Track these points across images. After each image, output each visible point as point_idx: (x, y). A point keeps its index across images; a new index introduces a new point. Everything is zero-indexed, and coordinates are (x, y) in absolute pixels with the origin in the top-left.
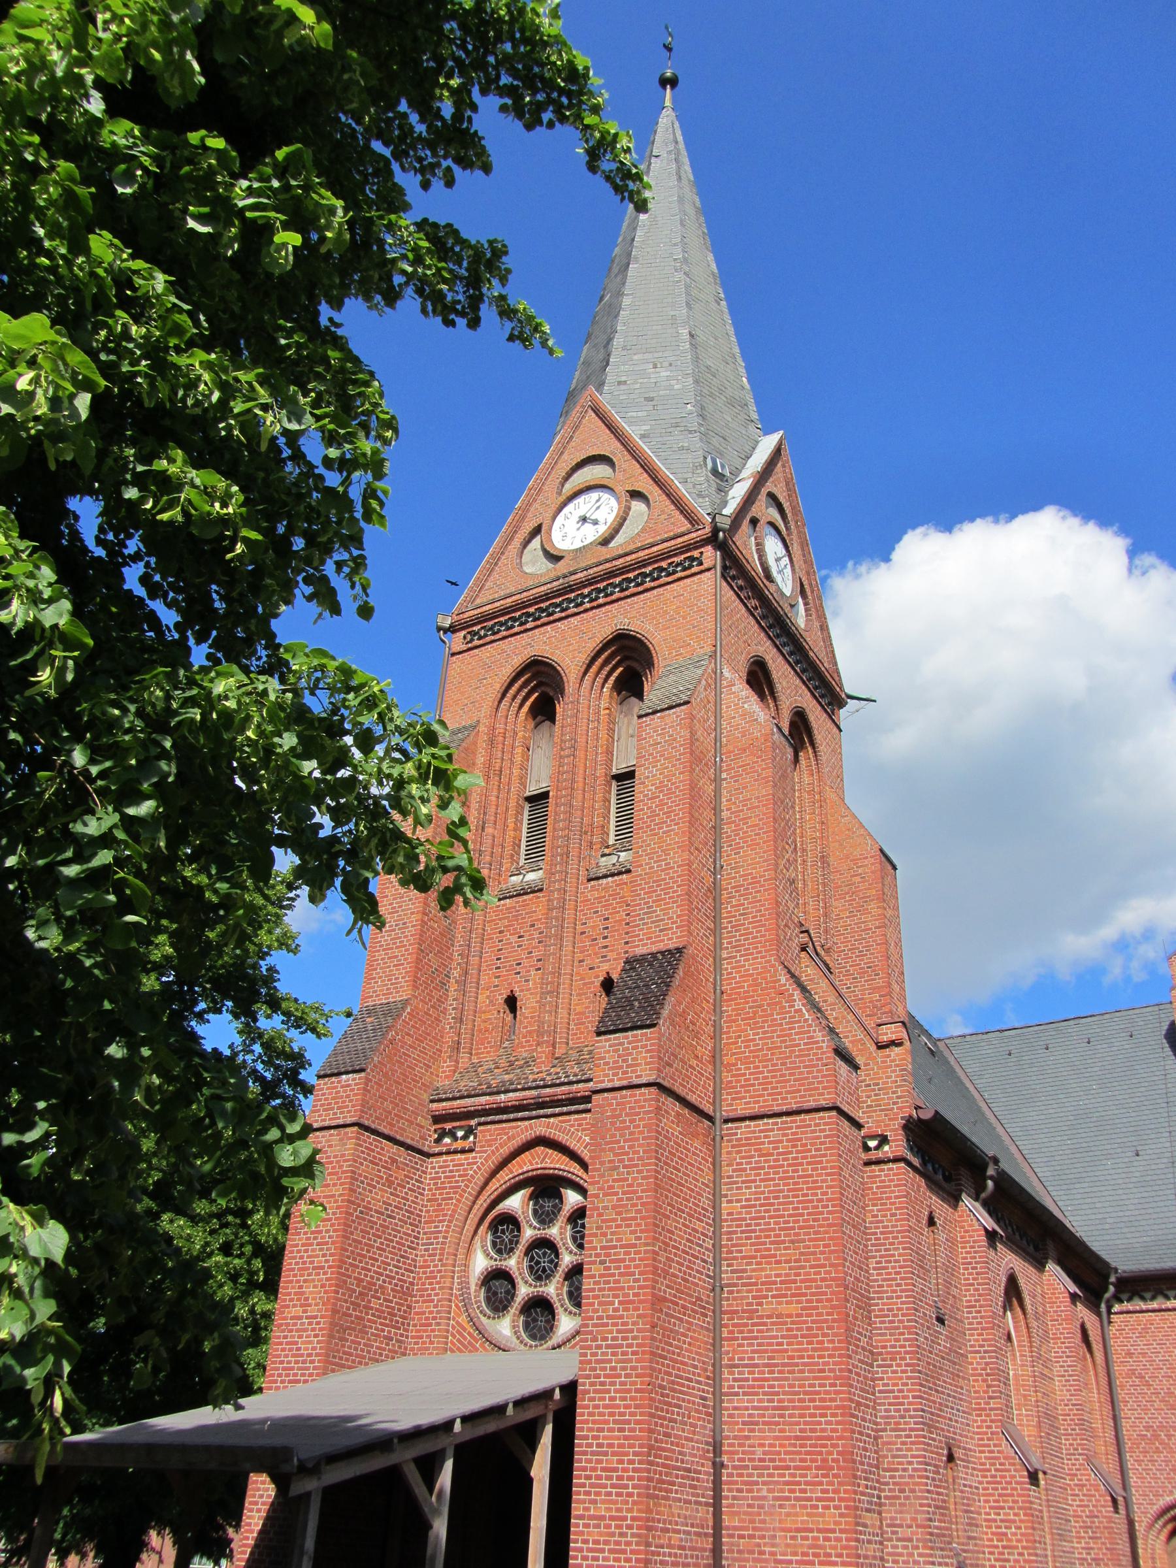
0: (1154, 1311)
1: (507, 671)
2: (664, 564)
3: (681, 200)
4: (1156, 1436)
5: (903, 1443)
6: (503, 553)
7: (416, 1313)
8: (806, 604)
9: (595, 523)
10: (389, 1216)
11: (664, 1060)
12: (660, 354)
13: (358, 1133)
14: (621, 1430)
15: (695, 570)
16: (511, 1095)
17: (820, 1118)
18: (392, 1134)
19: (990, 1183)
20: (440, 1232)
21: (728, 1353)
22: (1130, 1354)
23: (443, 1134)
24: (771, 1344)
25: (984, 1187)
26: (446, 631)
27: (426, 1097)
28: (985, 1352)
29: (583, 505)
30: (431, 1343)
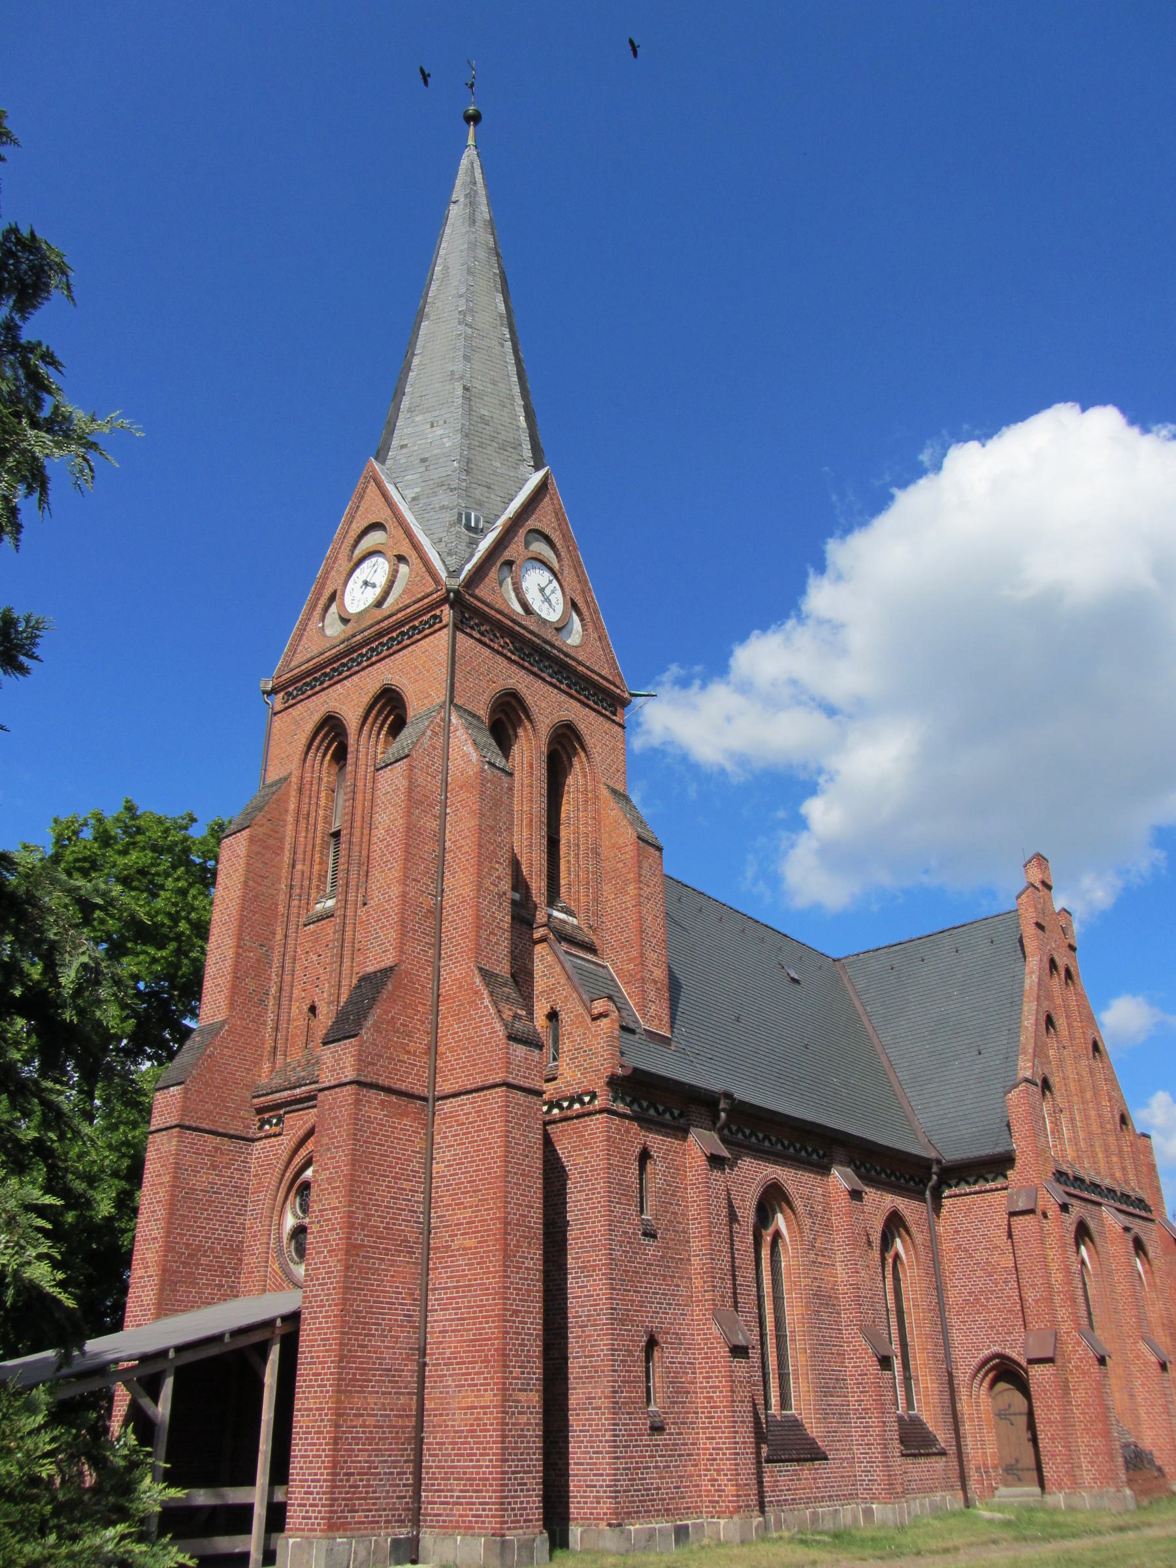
0: (976, 1193)
1: (310, 727)
2: (416, 623)
3: (473, 246)
4: (977, 1300)
5: (599, 1335)
6: (309, 619)
7: (246, 1264)
8: (582, 620)
9: (374, 586)
10: (215, 1193)
11: (362, 1061)
12: (437, 413)
13: (179, 1132)
14: (324, 1345)
15: (437, 626)
16: (303, 1088)
17: (496, 1093)
18: (214, 1128)
19: (723, 1115)
20: (260, 1200)
21: (432, 1279)
22: (957, 1232)
23: (263, 1122)
24: (458, 1271)
25: (718, 1117)
26: (269, 693)
27: (248, 1094)
28: (703, 1255)
29: (360, 574)
30: (254, 1286)
